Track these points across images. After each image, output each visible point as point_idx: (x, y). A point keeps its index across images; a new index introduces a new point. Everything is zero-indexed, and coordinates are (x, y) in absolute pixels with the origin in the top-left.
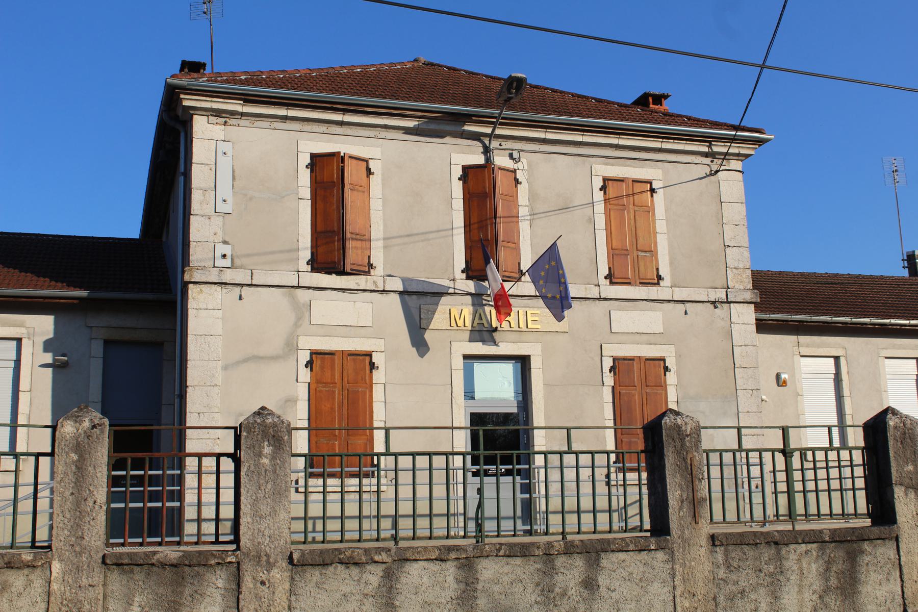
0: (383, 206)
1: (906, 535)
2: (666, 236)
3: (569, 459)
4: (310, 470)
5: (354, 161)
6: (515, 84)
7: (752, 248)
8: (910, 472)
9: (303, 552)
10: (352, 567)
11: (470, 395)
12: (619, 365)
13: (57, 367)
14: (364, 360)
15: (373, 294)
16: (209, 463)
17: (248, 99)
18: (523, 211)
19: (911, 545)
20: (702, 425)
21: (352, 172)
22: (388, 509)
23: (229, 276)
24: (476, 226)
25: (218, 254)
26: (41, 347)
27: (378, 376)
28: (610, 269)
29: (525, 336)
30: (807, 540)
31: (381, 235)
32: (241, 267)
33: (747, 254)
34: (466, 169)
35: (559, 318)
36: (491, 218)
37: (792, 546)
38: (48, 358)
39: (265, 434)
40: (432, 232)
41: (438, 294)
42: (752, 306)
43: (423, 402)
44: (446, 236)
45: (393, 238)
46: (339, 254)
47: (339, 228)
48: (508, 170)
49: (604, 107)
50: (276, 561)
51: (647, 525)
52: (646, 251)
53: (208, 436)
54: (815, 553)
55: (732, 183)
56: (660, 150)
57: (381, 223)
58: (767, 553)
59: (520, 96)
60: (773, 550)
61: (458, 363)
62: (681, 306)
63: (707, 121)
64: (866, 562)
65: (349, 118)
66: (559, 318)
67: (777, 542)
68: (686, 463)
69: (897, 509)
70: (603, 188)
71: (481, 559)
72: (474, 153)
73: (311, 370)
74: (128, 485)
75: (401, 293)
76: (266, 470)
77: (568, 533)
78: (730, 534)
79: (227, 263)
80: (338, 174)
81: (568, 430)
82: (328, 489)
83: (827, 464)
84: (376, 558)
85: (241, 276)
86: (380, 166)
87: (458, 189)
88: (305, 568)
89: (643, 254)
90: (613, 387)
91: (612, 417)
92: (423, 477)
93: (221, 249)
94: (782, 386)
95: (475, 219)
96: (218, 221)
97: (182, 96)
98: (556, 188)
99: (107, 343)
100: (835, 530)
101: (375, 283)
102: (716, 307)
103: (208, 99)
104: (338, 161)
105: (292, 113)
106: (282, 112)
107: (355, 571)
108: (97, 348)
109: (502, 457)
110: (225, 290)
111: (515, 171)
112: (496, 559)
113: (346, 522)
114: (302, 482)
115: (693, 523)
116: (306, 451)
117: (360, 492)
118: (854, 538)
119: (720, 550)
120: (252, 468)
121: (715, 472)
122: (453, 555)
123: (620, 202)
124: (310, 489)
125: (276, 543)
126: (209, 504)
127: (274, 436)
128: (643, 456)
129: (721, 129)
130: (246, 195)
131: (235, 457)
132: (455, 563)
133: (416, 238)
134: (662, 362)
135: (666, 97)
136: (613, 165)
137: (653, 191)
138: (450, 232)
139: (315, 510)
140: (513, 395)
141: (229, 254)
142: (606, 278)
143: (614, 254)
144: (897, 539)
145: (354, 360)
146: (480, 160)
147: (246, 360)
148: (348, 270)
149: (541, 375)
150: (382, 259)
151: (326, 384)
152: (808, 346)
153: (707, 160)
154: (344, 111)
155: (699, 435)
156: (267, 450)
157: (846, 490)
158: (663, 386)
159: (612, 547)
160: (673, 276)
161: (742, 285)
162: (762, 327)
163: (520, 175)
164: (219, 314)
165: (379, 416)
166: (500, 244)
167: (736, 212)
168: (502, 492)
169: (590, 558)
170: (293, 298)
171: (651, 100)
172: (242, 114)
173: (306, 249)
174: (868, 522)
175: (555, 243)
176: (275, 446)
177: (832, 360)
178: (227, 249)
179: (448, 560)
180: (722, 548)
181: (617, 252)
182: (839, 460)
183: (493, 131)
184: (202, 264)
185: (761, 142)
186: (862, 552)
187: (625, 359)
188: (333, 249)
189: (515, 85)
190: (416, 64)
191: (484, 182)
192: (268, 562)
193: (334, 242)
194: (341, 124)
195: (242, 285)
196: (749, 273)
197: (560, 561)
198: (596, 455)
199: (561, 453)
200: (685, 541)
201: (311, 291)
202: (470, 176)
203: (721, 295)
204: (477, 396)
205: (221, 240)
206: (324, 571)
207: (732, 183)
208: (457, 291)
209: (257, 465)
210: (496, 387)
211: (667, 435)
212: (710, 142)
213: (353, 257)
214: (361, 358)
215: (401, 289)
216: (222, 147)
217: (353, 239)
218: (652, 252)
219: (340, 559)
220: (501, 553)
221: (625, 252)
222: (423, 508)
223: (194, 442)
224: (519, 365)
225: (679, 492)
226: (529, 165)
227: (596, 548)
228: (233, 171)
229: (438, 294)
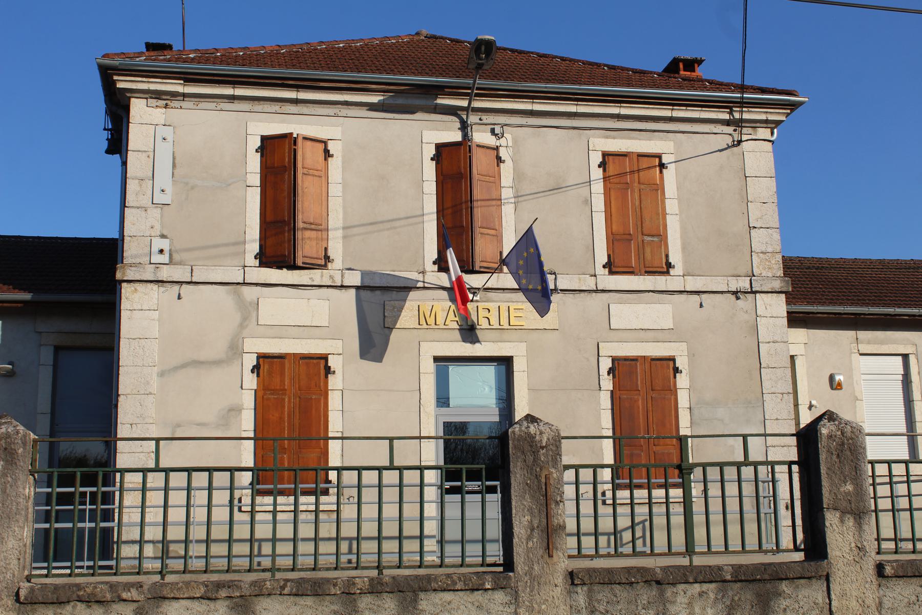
0: (343, 192)
3: (748, 472)
5: (309, 143)
6: (484, 48)
7: (784, 228)
8: (848, 493)
9: (32, 590)
14: (319, 364)
15: (330, 290)
16: (730, 473)
17: (189, 78)
18: (507, 193)
21: (307, 156)
23: (165, 273)
24: (450, 211)
25: (155, 249)
27: (334, 382)
28: (609, 256)
29: (506, 335)
30: (701, 578)
33: (776, 236)
34: (440, 147)
35: (543, 311)
36: (466, 202)
37: (681, 587)
41: (405, 288)
43: (388, 413)
44: (416, 224)
47: (289, 218)
48: (488, 148)
49: (640, 76)
52: (653, 236)
53: (141, 450)
56: (671, 119)
57: (341, 211)
58: (646, 594)
60: (654, 591)
61: (429, 367)
63: (732, 85)
65: (303, 95)
66: (543, 311)
67: (660, 581)
69: (828, 540)
70: (603, 165)
71: (261, 598)
72: (449, 129)
73: (258, 376)
74: (77, 503)
75: (358, 288)
77: (384, 568)
78: (770, 564)
79: (165, 258)
81: (391, 439)
83: (890, 479)
84: (125, 595)
87: (430, 170)
88: (36, 606)
89: (650, 239)
90: (612, 392)
91: (610, 426)
92: (390, 495)
93: (158, 244)
94: (836, 389)
96: (155, 213)
97: (115, 78)
98: (547, 169)
99: (57, 349)
100: (741, 566)
101: (331, 277)
102: (738, 298)
103: (144, 79)
105: (240, 91)
106: (228, 91)
108: (47, 355)
109: (83, 475)
110: (162, 289)
111: (497, 149)
112: (280, 598)
115: (546, 556)
116: (612, 462)
117: (317, 512)
118: (766, 577)
122: (223, 593)
124: (257, 508)
126: (350, 521)
127: (6, 449)
128: (795, 468)
129: (721, 91)
130: (187, 184)
132: (227, 603)
133: (381, 226)
134: (671, 363)
135: (700, 62)
136: (614, 138)
137: (662, 166)
138: (420, 219)
141: (167, 249)
142: (604, 267)
143: (613, 239)
144: (828, 578)
146: (457, 137)
147: (184, 366)
149: (526, 379)
151: (274, 392)
152: (869, 343)
153: (730, 129)
154: (298, 88)
155: (558, 447)
158: (674, 391)
159: (434, 585)
160: (685, 262)
161: (770, 271)
162: (795, 320)
163: (503, 153)
164: (156, 315)
165: (335, 425)
168: (480, 511)
169: (405, 599)
170: (239, 296)
171: (681, 66)
172: (185, 96)
173: (254, 241)
174: (799, 556)
175: (530, 229)
177: (900, 358)
178: (165, 244)
179: (216, 599)
180: (585, 588)
181: (618, 237)
183: (470, 104)
184: (138, 261)
185: (793, 106)
186: (779, 594)
187: (626, 359)
188: (281, 243)
189: (483, 48)
190: (416, 38)
194: (296, 102)
195: (181, 283)
196: (779, 258)
197: (365, 602)
198: (893, 465)
200: (533, 578)
201: (259, 288)
202: (444, 156)
203: (744, 284)
204: (452, 402)
205: (159, 233)
206: (59, 611)
207: (758, 155)
208: (426, 285)
210: (475, 395)
211: (515, 447)
213: (306, 248)
214: (315, 361)
216: (162, 131)
217: (306, 229)
218: (662, 237)
219: (78, 596)
220: (286, 591)
221: (628, 237)
222: (391, 529)
225: (528, 518)
226: (515, 141)
228: (174, 158)
229: (405, 288)
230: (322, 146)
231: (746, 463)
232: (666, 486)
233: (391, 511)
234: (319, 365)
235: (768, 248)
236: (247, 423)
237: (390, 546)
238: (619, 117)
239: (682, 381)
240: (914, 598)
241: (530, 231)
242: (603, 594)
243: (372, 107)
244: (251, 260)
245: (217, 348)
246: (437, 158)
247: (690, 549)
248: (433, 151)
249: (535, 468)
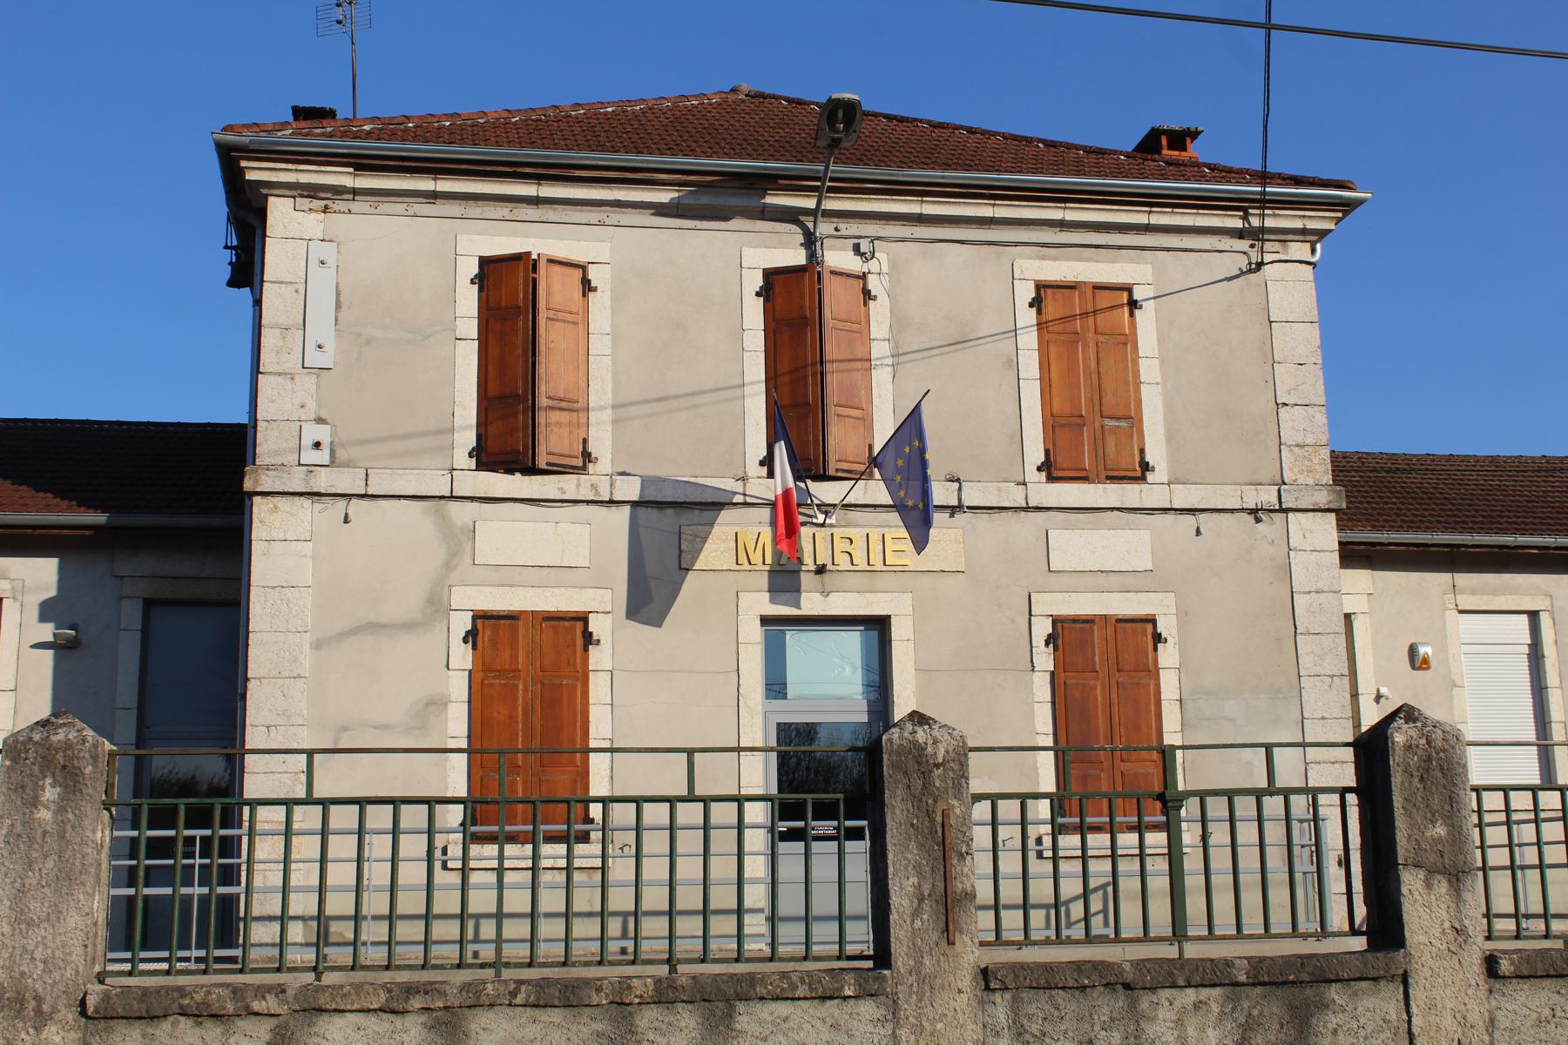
1: (1426, 972)
2: (1159, 389)
3: (1273, 805)
4: (473, 829)
5: (557, 269)
6: (843, 113)
7: (1332, 408)
9: (106, 996)
10: (209, 1023)
11: (776, 688)
12: (1065, 633)
13: (62, 648)
14: (573, 628)
15: (592, 508)
16: (1217, 807)
17: (362, 164)
18: (880, 350)
19: (1437, 993)
20: (971, 744)
21: (555, 290)
22: (621, 900)
23: (323, 481)
24: (787, 378)
25: (307, 441)
26: (35, 613)
27: (599, 658)
28: (1047, 452)
29: (879, 581)
31: (608, 399)
32: (349, 464)
33: (1321, 418)
34: (769, 274)
37: (1165, 993)
38: (47, 632)
39: (47, 764)
40: (705, 392)
41: (715, 505)
42: (1333, 515)
43: (686, 705)
45: (631, 404)
46: (525, 435)
48: (849, 275)
50: (55, 1010)
52: (1118, 419)
53: (283, 768)
54: (1215, 1008)
55: (1291, 285)
57: (609, 378)
58: (1107, 1005)
59: (854, 136)
60: (1120, 1001)
61: (753, 633)
62: (1189, 520)
63: (1247, 171)
64: (1331, 1026)
67: (1130, 984)
68: (932, 821)
69: (1405, 917)
70: (1036, 303)
71: (478, 1011)
73: (474, 647)
75: (634, 504)
76: (45, 833)
77: (679, 961)
79: (323, 456)
80: (526, 292)
81: (690, 752)
82: (507, 864)
84: (256, 1006)
85: (347, 481)
86: (608, 276)
87: (754, 313)
88: (112, 1023)
89: (1114, 423)
90: (1052, 673)
91: (1050, 729)
93: (313, 432)
94: (1420, 668)
95: (784, 367)
96: (307, 383)
97: (244, 164)
98: (940, 308)
99: (149, 604)
100: (1262, 960)
101: (594, 487)
102: (1258, 520)
103: (290, 166)
104: (526, 270)
106: (426, 184)
107: (213, 1031)
108: (132, 615)
110: (318, 506)
112: (509, 1011)
113: (713, 920)
114: (1047, 841)
115: (944, 943)
117: (569, 869)
118: (1305, 977)
119: (1002, 1001)
120: (18, 828)
121: (982, 836)
122: (416, 1003)
123: (1068, 327)
124: (472, 864)
125: (56, 975)
126: (268, 890)
127: (64, 767)
128: (1352, 799)
132: (423, 1018)
134: (1149, 627)
135: (1195, 135)
136: (1055, 259)
137: (1133, 304)
138: (738, 392)
139: (482, 901)
140: (860, 689)
142: (1039, 469)
143: (1054, 425)
145: (554, 628)
146: (798, 257)
147: (354, 631)
148: (831, 472)
150: (608, 443)
151: (501, 673)
152: (1474, 592)
153: (1244, 245)
154: (539, 179)
155: (963, 765)
156: (50, 793)
157: (1522, 868)
158: (1153, 672)
159: (760, 990)
161: (1311, 476)
162: (1352, 556)
163: (873, 284)
165: (600, 729)
166: (832, 410)
167: (1300, 341)
168: (835, 869)
169: (713, 1013)
170: (443, 519)
171: (1164, 141)
172: (355, 192)
174: (1359, 943)
175: (918, 406)
176: (67, 787)
178: (323, 433)
179: (404, 1012)
180: (1008, 996)
181: (1062, 421)
182: (1508, 810)
184: (279, 460)
185: (1348, 206)
186: (1325, 1006)
187: (1076, 620)
188: (512, 430)
189: (840, 114)
190: (732, 97)
191: (802, 298)
192: (39, 1011)
193: (516, 414)
194: (536, 201)
195: (349, 496)
196: (1325, 454)
197: (647, 1018)
199: (672, 801)
201: (476, 505)
202: (777, 289)
203: (1268, 497)
205: (313, 416)
206: (150, 1030)
207: (1291, 285)
208: (749, 500)
209: (29, 823)
210: (829, 680)
212: (1245, 210)
213: (553, 439)
214: (567, 624)
215: (636, 498)
216: (319, 251)
218: (1133, 420)
219: (181, 1007)
220: (520, 999)
221: (1078, 420)
222: (689, 898)
224: (874, 634)
225: (914, 880)
226: (893, 264)
227: (724, 994)
228: (338, 294)
229: (715, 505)
230: (578, 274)
231: (1271, 790)
232: (1140, 828)
233: (689, 869)
234: (573, 630)
235: (1306, 440)
236: (456, 726)
237: (551, 929)
238: (1062, 225)
239: (1168, 656)
240: (1547, 1012)
241: (916, 413)
242: (1037, 1006)
243: (660, 210)
244: (463, 459)
245: (407, 602)
246: (766, 292)
247: (1179, 932)
248: (474, 269)
249: (925, 800)
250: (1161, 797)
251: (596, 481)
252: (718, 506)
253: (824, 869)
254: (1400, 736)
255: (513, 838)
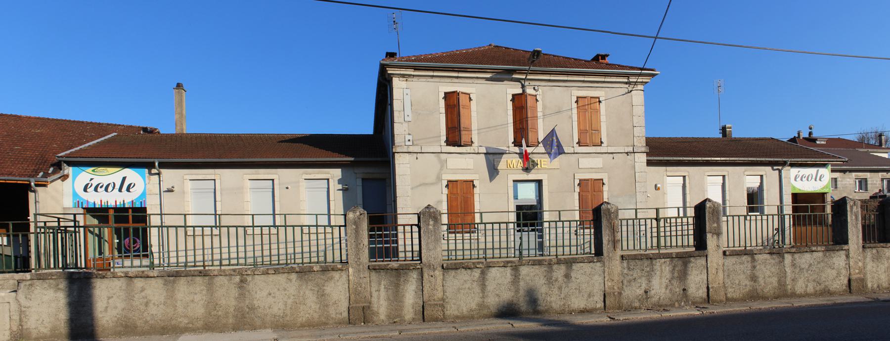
3: (560, 224)
6: (536, 54)
7: (647, 126)
12: (582, 183)
13: (344, 190)
17: (416, 68)
18: (540, 114)
21: (463, 100)
23: (411, 149)
27: (476, 190)
34: (514, 95)
38: (340, 187)
39: (430, 216)
43: (495, 202)
49: (578, 62)
51: (593, 252)
55: (638, 96)
56: (604, 82)
58: (646, 263)
60: (649, 261)
61: (511, 184)
65: (461, 75)
67: (651, 258)
70: (577, 102)
79: (410, 143)
81: (185, 215)
87: (510, 105)
93: (408, 137)
95: (518, 119)
96: (406, 125)
98: (555, 102)
99: (363, 179)
105: (436, 74)
106: (431, 73)
107: (469, 271)
108: (359, 182)
131: (418, 226)
135: (607, 56)
143: (581, 132)
146: (520, 91)
147: (420, 185)
153: (627, 86)
154: (458, 71)
158: (602, 192)
161: (641, 144)
162: (650, 163)
165: (477, 208)
174: (694, 249)
178: (410, 137)
188: (455, 135)
194: (457, 77)
197: (555, 267)
203: (631, 149)
207: (638, 96)
210: (527, 194)
213: (464, 139)
216: (406, 91)
218: (598, 131)
222: (497, 245)
223: (401, 220)
231: (679, 217)
233: (497, 239)
234: (471, 184)
235: (640, 134)
237: (467, 253)
238: (584, 81)
239: (605, 188)
241: (553, 131)
242: (632, 263)
243: (487, 79)
245: (432, 178)
246: (513, 100)
247: (658, 246)
249: (610, 220)
250: (656, 219)
251: (474, 148)
252: (503, 154)
253: (525, 239)
254: (708, 205)
255: (458, 233)
